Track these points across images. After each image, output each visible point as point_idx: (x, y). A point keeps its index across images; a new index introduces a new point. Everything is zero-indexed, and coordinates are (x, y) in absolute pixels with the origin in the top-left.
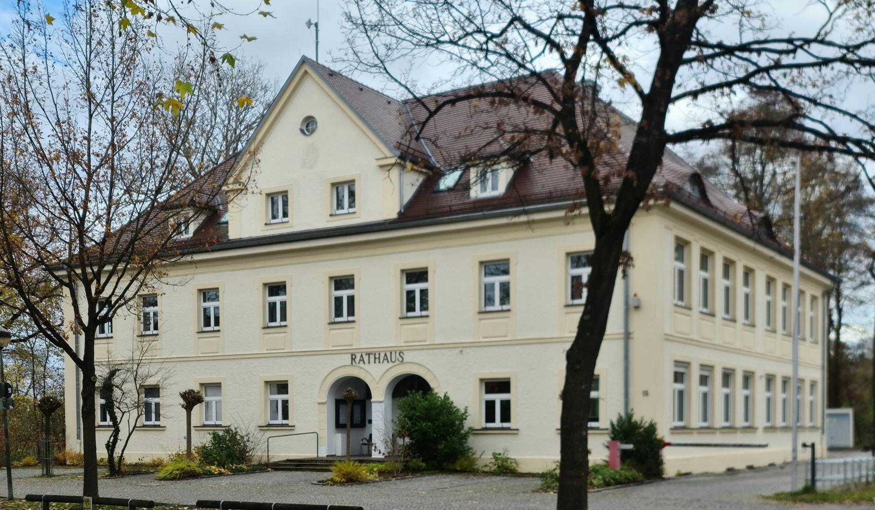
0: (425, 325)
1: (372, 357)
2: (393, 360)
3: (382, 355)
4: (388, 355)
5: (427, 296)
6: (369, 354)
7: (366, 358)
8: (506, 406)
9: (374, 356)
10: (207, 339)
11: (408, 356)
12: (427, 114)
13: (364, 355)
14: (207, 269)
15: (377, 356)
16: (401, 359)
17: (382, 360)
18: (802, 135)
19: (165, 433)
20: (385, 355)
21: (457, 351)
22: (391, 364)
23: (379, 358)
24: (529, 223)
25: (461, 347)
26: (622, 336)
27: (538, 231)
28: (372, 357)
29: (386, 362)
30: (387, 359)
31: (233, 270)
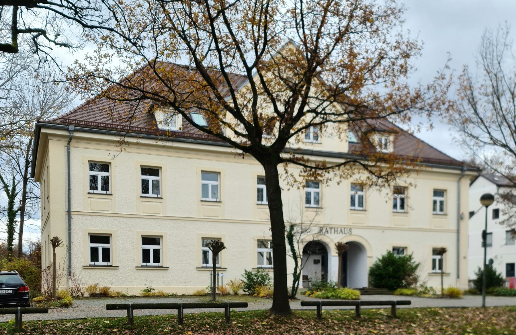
0: (160, 204)
1: (333, 230)
2: (346, 232)
3: (339, 229)
4: (343, 230)
5: (258, 196)
6: (331, 228)
7: (329, 231)
8: (157, 253)
9: (333, 229)
10: (212, 207)
11: (354, 231)
12: (21, 26)
13: (328, 228)
14: (211, 158)
15: (336, 229)
16: (350, 233)
17: (339, 232)
18: (511, 191)
19: (168, 272)
20: (341, 230)
21: (381, 231)
22: (344, 235)
23: (337, 231)
24: (121, 143)
25: (383, 229)
26: (72, 213)
27: (129, 149)
28: (333, 230)
29: (341, 233)
30: (342, 232)
31: (233, 162)
